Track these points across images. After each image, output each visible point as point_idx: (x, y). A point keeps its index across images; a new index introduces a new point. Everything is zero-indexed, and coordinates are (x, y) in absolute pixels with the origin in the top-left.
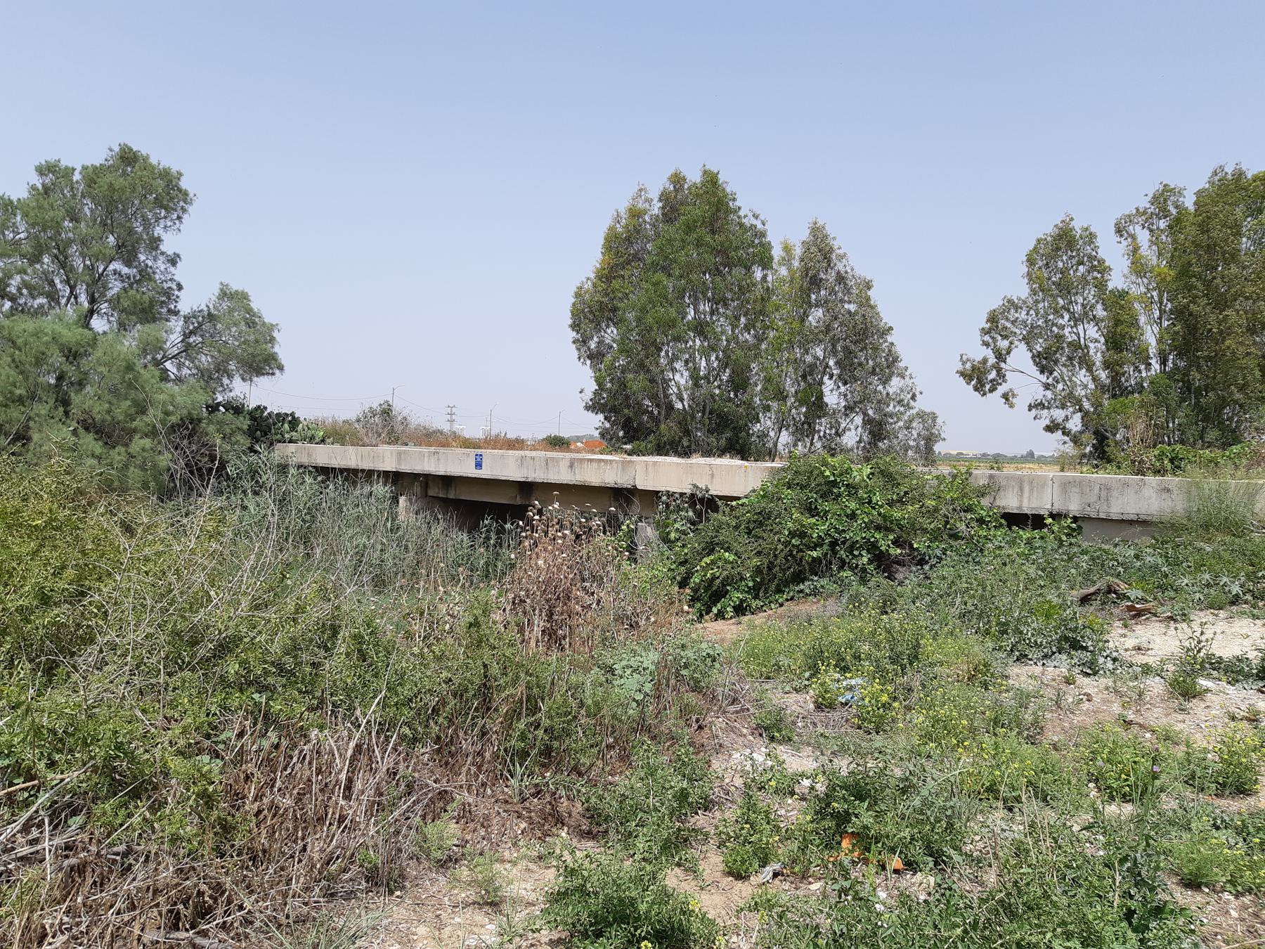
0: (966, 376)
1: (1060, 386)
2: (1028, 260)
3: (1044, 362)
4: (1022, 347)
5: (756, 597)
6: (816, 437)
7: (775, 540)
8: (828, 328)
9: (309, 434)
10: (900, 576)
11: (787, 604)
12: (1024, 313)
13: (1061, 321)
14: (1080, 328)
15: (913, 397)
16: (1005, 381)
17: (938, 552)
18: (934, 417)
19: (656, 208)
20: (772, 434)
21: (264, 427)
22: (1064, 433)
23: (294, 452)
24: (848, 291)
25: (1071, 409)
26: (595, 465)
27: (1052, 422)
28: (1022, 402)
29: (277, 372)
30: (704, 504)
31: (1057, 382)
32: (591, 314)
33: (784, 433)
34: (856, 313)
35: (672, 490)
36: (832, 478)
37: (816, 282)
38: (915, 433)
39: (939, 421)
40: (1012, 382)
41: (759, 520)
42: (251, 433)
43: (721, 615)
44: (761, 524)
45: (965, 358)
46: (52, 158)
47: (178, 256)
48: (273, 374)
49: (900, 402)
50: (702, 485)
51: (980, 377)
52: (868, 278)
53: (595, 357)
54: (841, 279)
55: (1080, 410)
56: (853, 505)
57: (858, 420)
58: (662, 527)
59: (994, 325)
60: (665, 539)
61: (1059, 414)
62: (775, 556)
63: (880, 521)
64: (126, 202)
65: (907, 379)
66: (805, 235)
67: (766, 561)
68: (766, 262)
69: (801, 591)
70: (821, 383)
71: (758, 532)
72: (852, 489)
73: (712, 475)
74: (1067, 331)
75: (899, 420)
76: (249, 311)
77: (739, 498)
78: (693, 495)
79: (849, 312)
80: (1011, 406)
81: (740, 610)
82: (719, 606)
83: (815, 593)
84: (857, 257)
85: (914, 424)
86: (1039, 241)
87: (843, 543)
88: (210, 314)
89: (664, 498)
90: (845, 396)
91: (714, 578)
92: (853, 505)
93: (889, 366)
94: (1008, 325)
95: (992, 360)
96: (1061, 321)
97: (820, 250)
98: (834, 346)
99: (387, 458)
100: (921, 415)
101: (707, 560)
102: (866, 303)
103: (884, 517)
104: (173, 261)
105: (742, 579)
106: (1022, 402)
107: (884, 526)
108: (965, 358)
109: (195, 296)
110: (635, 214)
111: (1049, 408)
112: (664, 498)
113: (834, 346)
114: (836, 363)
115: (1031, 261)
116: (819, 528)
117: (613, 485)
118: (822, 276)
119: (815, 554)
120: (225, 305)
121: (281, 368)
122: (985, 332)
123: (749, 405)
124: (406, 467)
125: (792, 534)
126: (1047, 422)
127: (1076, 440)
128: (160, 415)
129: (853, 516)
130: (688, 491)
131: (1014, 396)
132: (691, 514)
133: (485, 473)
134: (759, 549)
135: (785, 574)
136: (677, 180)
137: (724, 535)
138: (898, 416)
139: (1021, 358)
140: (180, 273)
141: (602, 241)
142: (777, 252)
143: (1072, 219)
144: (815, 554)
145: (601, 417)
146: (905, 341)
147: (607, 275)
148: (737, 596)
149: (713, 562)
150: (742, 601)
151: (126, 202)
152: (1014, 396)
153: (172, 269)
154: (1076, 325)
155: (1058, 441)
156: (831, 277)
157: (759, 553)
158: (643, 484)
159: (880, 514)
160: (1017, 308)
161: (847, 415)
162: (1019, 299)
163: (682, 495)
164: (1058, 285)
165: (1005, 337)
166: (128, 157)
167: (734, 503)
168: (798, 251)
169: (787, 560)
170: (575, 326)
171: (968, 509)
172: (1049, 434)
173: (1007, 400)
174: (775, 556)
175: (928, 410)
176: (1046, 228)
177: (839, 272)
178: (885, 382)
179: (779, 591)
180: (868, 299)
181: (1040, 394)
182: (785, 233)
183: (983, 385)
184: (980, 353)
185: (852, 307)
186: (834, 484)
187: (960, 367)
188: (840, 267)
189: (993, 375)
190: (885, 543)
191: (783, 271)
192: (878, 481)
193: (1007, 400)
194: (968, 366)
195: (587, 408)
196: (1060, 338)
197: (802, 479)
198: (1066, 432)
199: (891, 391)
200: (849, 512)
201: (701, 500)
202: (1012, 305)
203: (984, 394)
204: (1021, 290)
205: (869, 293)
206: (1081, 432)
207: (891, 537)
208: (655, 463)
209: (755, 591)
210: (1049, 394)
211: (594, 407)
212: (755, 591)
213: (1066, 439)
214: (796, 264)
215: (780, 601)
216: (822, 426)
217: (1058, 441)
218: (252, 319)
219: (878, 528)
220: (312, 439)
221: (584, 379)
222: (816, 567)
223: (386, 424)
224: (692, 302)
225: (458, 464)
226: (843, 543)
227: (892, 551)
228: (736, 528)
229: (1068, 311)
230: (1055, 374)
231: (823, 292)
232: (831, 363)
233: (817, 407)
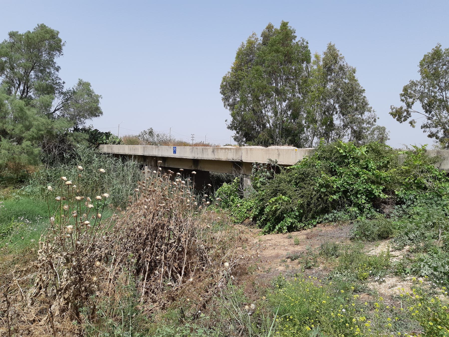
0: (393, 115)
1: (435, 118)
2: (420, 65)
3: (428, 108)
4: (418, 101)
5: (300, 221)
6: (330, 139)
7: (311, 189)
8: (336, 90)
9: (113, 140)
10: (386, 211)
11: (318, 225)
12: (419, 87)
13: (435, 90)
14: (444, 93)
15: (375, 121)
16: (410, 116)
17: (412, 197)
18: (384, 129)
19: (260, 40)
20: (310, 138)
21: (96, 138)
22: (436, 138)
23: (105, 149)
24: (344, 73)
25: (440, 128)
26: (224, 151)
27: (432, 133)
28: (418, 125)
29: (100, 115)
30: (274, 168)
31: (433, 116)
32: (230, 87)
33: (315, 138)
34: (348, 83)
35: (259, 162)
36: (344, 154)
37: (330, 70)
38: (375, 136)
39: (386, 130)
40: (414, 116)
41: (302, 177)
42: (90, 141)
43: (280, 230)
44: (303, 180)
45: (393, 107)
46: (15, 30)
47: (59, 67)
48: (99, 116)
49: (369, 123)
50: (274, 159)
51: (399, 115)
52: (354, 67)
53: (232, 106)
54: (341, 68)
55: (444, 128)
56: (357, 169)
57: (349, 131)
58: (254, 180)
59: (407, 93)
60: (255, 187)
61: (434, 130)
62: (311, 198)
63: (373, 178)
64: (41, 46)
65: (372, 112)
66: (325, 49)
67: (306, 201)
68: (307, 59)
69: (327, 219)
70: (332, 114)
71: (302, 184)
72: (356, 160)
73: (279, 155)
74: (437, 95)
75: (368, 130)
76: (89, 90)
77: (291, 166)
78: (269, 164)
79: (345, 83)
80: (414, 127)
81: (291, 229)
82: (279, 225)
83: (335, 220)
84: (349, 58)
85: (375, 133)
86: (425, 56)
87: (352, 191)
88: (74, 92)
89: (255, 166)
90: (343, 120)
91: (276, 210)
92: (357, 169)
93: (363, 107)
94: (412, 92)
95: (405, 107)
96: (435, 90)
97: (332, 56)
98: (338, 99)
99: (139, 150)
100: (379, 128)
101: (273, 199)
102: (352, 79)
103: (377, 177)
104: (58, 69)
105: (292, 211)
106: (418, 125)
107: (376, 182)
108: (393, 107)
109: (69, 83)
110: (250, 43)
111: (429, 128)
112: (255, 166)
113: (338, 99)
114: (339, 106)
115: (421, 65)
116: (337, 183)
117: (232, 160)
118: (333, 67)
119: (335, 197)
120: (81, 87)
121: (101, 113)
122: (402, 95)
123: (300, 125)
124: (146, 154)
125: (321, 186)
126: (429, 133)
127: (442, 141)
128: (35, 131)
129: (357, 175)
130: (267, 163)
131: (415, 123)
132: (268, 174)
133: (177, 155)
134: (302, 194)
135: (318, 208)
136: (270, 27)
137: (283, 186)
138: (368, 129)
139: (418, 106)
140: (60, 74)
141: (235, 55)
142: (313, 59)
143: (440, 46)
144: (335, 197)
145: (235, 132)
146: (370, 96)
147: (238, 68)
148: (289, 220)
149: (276, 201)
150: (292, 223)
151: (41, 46)
152: (415, 123)
153: (57, 73)
154: (442, 92)
155: (434, 141)
156: (337, 68)
157: (302, 196)
158: (246, 159)
159: (373, 174)
160: (416, 85)
161: (344, 129)
162: (417, 81)
163: (264, 164)
164: (433, 74)
165: (411, 97)
166: (42, 27)
167: (288, 168)
168: (322, 56)
169: (318, 201)
170: (223, 93)
171: (428, 171)
172: (430, 138)
173: (412, 124)
174: (311, 198)
175: (381, 126)
176: (429, 50)
177: (340, 65)
178: (362, 114)
179: (313, 218)
180: (354, 77)
181: (425, 121)
182: (317, 50)
183: (401, 118)
184: (400, 104)
185: (347, 81)
186: (346, 157)
187: (390, 111)
188: (341, 63)
189: (405, 114)
190: (378, 191)
191: (315, 67)
192: (371, 155)
193: (412, 124)
194: (394, 110)
195: (229, 128)
196: (434, 97)
197: (327, 155)
198: (437, 138)
199: (364, 118)
200: (355, 173)
201: (273, 167)
202: (413, 84)
203: (401, 122)
204: (418, 77)
205: (354, 75)
206: (444, 137)
207: (381, 188)
208: (251, 149)
209: (300, 218)
210: (430, 122)
211: (230, 128)
212: (300, 218)
213: (438, 140)
214: (321, 63)
215: (315, 223)
216: (333, 134)
217: (434, 141)
218: (90, 93)
219: (373, 182)
220: (114, 143)
221: (226, 116)
222: (336, 205)
223: (149, 137)
224: (275, 79)
225: (166, 152)
226: (352, 191)
227: (381, 195)
228: (290, 181)
229: (438, 85)
230: (433, 113)
231: (333, 74)
232: (337, 106)
233: (330, 126)
